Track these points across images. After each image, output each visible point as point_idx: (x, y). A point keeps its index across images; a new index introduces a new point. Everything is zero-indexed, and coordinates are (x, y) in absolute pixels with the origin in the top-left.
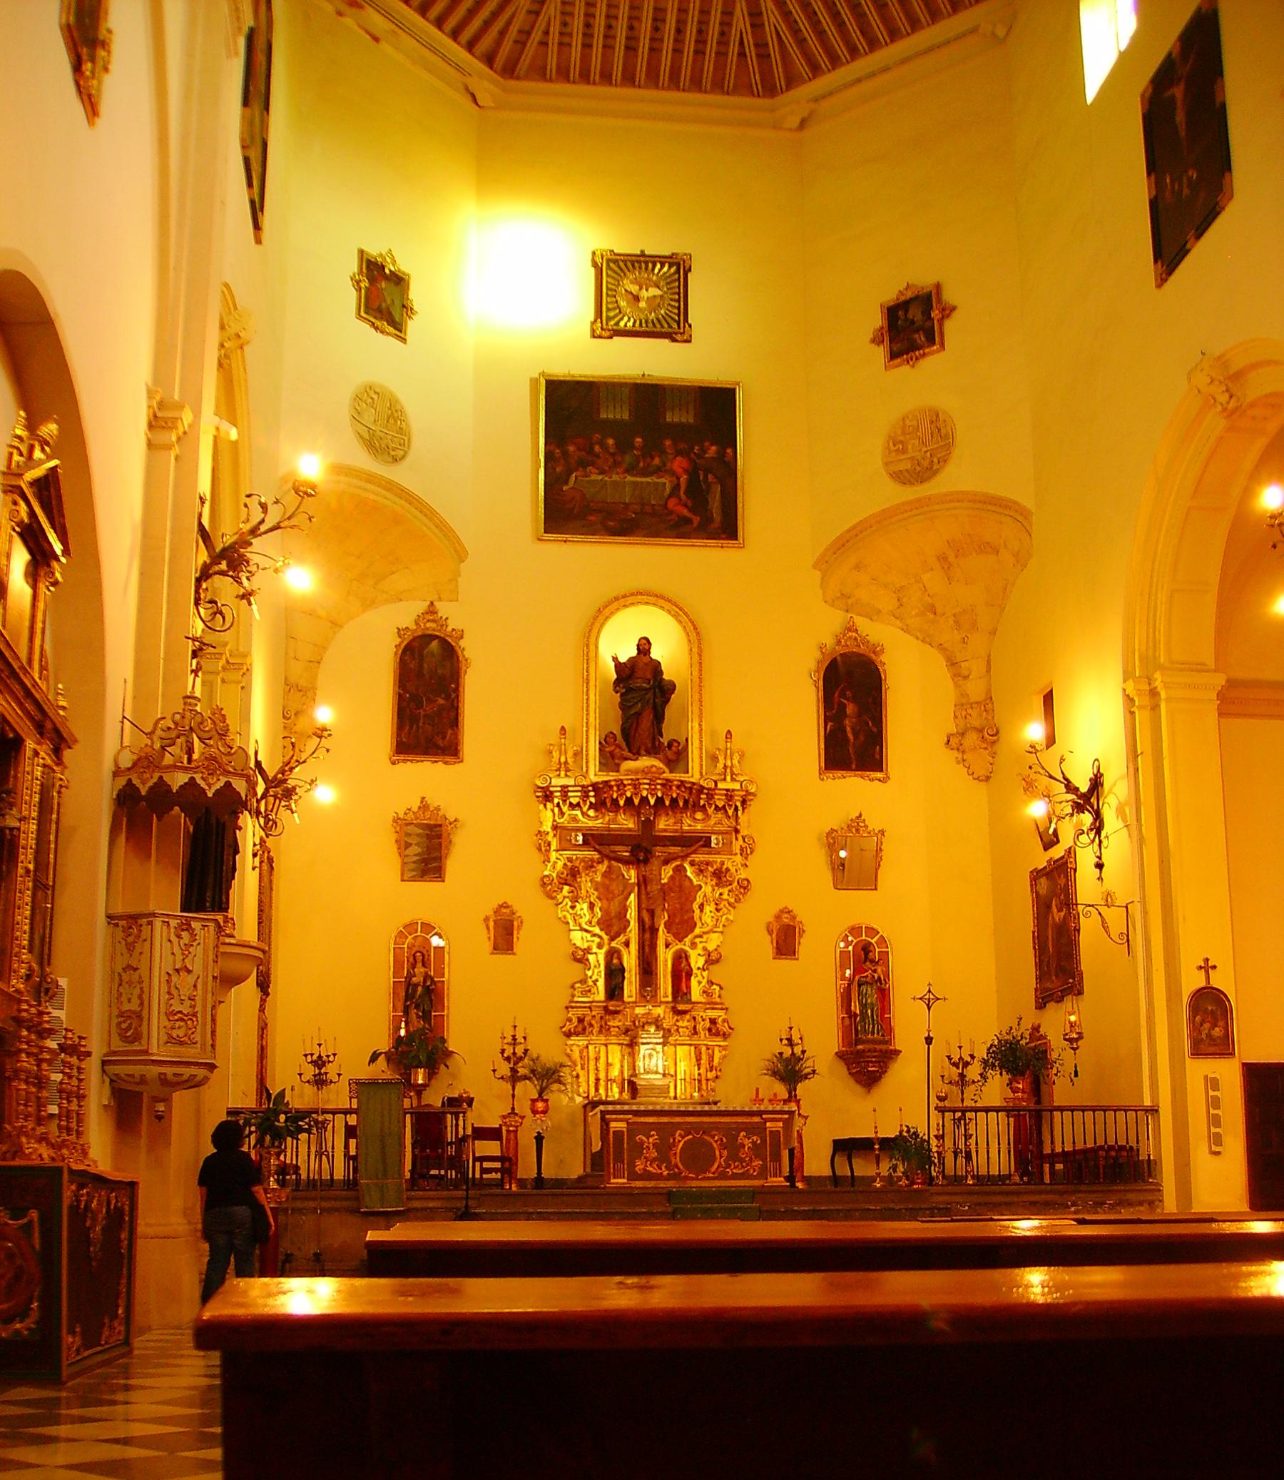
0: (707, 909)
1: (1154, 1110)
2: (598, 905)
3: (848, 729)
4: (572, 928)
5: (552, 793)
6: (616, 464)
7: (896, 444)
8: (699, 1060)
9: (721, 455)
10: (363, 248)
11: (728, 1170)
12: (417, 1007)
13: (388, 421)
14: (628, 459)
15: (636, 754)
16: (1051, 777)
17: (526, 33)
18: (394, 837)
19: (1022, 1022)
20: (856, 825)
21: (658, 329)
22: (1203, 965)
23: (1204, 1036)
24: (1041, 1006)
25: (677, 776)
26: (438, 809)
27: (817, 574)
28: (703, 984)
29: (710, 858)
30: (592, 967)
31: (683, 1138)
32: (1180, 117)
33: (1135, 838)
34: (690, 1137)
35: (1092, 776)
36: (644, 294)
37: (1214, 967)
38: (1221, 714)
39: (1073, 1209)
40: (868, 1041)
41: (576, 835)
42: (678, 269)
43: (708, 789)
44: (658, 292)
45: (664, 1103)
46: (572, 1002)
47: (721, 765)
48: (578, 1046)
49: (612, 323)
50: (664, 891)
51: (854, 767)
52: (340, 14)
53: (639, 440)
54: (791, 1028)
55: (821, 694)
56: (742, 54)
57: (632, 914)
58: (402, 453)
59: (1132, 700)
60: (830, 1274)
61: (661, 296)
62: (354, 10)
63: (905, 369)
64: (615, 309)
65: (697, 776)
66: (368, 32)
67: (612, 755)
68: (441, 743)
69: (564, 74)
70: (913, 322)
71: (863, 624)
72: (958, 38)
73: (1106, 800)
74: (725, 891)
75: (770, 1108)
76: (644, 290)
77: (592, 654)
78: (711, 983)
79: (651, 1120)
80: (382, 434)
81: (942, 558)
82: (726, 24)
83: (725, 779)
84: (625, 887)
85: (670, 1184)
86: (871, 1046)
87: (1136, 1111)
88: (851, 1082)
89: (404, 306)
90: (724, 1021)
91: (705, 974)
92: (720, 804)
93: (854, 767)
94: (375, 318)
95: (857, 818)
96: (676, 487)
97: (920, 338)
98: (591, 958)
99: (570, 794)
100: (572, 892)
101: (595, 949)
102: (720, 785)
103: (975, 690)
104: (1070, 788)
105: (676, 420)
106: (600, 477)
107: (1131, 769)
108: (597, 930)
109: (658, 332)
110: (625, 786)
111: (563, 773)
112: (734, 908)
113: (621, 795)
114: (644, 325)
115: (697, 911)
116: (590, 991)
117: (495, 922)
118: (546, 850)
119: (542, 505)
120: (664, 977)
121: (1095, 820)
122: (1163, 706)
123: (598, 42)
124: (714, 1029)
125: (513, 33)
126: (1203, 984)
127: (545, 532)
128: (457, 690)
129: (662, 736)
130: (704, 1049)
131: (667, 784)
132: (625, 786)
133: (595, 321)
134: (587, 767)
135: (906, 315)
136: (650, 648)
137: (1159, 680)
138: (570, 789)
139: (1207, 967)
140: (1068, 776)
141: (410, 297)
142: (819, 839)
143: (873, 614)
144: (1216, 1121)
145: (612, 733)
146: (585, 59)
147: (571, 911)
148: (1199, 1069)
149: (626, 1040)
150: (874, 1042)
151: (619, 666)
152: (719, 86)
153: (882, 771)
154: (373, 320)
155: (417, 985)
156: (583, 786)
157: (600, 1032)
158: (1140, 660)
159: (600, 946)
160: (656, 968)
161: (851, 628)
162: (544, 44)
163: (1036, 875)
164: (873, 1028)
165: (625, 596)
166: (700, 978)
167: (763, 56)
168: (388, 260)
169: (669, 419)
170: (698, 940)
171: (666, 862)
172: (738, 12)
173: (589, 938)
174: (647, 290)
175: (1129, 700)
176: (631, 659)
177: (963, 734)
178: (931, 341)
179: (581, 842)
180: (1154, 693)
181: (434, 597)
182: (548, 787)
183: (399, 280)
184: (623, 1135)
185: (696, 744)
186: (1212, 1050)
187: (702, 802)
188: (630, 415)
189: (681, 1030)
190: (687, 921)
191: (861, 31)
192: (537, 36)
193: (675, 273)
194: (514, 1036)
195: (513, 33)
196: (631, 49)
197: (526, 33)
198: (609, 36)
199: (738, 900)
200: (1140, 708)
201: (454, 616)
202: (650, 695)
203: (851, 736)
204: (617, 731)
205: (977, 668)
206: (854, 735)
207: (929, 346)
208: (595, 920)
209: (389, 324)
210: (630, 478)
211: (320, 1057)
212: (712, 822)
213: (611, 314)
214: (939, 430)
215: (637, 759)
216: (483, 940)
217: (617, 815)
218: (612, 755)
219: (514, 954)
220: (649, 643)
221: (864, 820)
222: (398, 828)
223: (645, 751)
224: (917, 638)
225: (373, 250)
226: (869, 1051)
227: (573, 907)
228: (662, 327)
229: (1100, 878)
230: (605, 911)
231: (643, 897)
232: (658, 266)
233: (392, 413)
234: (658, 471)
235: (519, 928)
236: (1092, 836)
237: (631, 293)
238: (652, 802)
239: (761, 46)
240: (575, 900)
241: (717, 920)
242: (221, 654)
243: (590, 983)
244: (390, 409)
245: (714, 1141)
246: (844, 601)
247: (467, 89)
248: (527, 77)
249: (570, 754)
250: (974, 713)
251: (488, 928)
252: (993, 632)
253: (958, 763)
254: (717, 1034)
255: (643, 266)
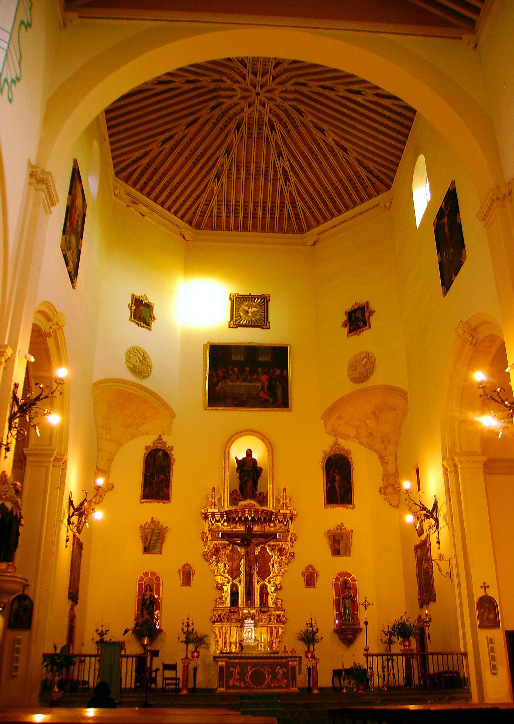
0: (276, 565)
1: (465, 654)
2: (228, 564)
3: (337, 487)
4: (216, 574)
5: (208, 515)
6: (238, 378)
7: (353, 367)
8: (271, 633)
9: (282, 373)
10: (134, 293)
11: (271, 684)
12: (147, 609)
13: (142, 362)
14: (243, 376)
15: (245, 499)
16: (415, 504)
17: (204, 213)
18: (140, 534)
19: (406, 614)
20: (341, 527)
21: (256, 324)
22: (483, 585)
23: (485, 618)
24: (421, 607)
25: (263, 508)
26: (159, 522)
27: (322, 422)
28: (274, 599)
29: (277, 543)
30: (225, 591)
31: (251, 669)
32: (446, 229)
33: (451, 529)
34: (254, 669)
35: (434, 503)
36: (250, 310)
37: (488, 587)
38: (485, 474)
39: (429, 702)
40: (347, 625)
41: (218, 534)
42: (264, 301)
43: (275, 513)
44: (256, 309)
45: (254, 653)
46: (216, 607)
47: (281, 503)
48: (218, 627)
49: (237, 322)
50: (256, 558)
51: (339, 502)
52: (128, 206)
53: (247, 368)
54: (311, 619)
55: (325, 472)
56: (289, 218)
57: (242, 569)
58: (148, 374)
59: (447, 469)
60: (105, 709)
61: (257, 311)
62: (135, 205)
63: (355, 337)
64: (238, 316)
65: (271, 507)
66: (140, 213)
67: (235, 499)
68: (162, 494)
69: (219, 227)
70: (358, 318)
71: (341, 441)
72: (372, 208)
73: (440, 513)
74: (284, 557)
75: (290, 655)
76: (250, 309)
77: (227, 456)
78: (277, 599)
79: (237, 661)
80: (139, 367)
81: (374, 413)
82: (282, 207)
83: (283, 509)
84: (239, 556)
85: (245, 691)
86: (347, 627)
87: (457, 654)
88: (340, 643)
89: (150, 316)
90: (283, 616)
91: (274, 594)
92: (281, 520)
93: (339, 502)
94: (138, 321)
95: (341, 525)
96: (263, 387)
97: (361, 324)
98: (225, 588)
99: (216, 516)
100: (216, 558)
101: (226, 584)
102: (281, 511)
103: (391, 468)
104: (423, 508)
105: (263, 360)
106: (231, 383)
107: (448, 499)
108: (227, 575)
109: (259, 325)
110: (238, 512)
111: (213, 507)
112: (288, 565)
113: (237, 516)
114: (250, 322)
115: (271, 567)
116: (224, 602)
117: (183, 572)
118: (205, 540)
119: (207, 395)
120: (257, 596)
121: (436, 522)
122: (459, 471)
123: (232, 215)
124: (278, 619)
125: (199, 212)
126: (483, 594)
127: (208, 406)
128: (169, 472)
129: (257, 491)
130: (274, 628)
131: (256, 511)
132: (238, 512)
133: (230, 321)
134: (224, 504)
135: (355, 315)
136: (252, 453)
137: (457, 460)
138: (215, 513)
139: (485, 587)
140: (423, 503)
141: (153, 313)
142: (325, 534)
143: (346, 437)
144: (493, 658)
145: (235, 489)
146: (228, 222)
147: (216, 567)
148: (484, 634)
149: (239, 625)
150: (350, 625)
151: (238, 461)
152: (281, 230)
153: (352, 504)
154: (137, 322)
155: (147, 600)
156: (221, 513)
157: (228, 621)
158: (449, 452)
159: (228, 582)
160: (253, 592)
161: (337, 443)
162: (211, 216)
163: (417, 548)
164: (349, 618)
165: (241, 432)
166: (272, 596)
167: (298, 218)
168: (145, 298)
169: (260, 360)
170: (271, 580)
171: (257, 545)
172: (286, 202)
173: (224, 579)
174: (251, 309)
175: (445, 469)
176: (244, 459)
177: (386, 488)
178: (365, 325)
179: (220, 537)
180: (455, 466)
181: (161, 433)
182: (206, 513)
183: (149, 306)
184: (224, 668)
185: (271, 493)
186: (489, 625)
187: (273, 519)
188: (244, 357)
189: (263, 620)
190: (266, 571)
191: (334, 208)
192: (208, 213)
193: (263, 302)
194: (188, 623)
195: (199, 212)
196: (245, 217)
197: (204, 213)
198: (236, 213)
199: (289, 562)
200: (450, 472)
201: (169, 441)
202: (251, 473)
203: (338, 490)
204: (238, 489)
205: (391, 459)
206: (339, 489)
207: (364, 327)
208: (226, 571)
209: (144, 323)
210: (244, 384)
211: (102, 631)
212: (278, 527)
213: (237, 318)
214: (369, 360)
215: (245, 501)
216: (177, 580)
217: (236, 525)
218: (235, 499)
219: (191, 586)
220: (251, 452)
221: (344, 526)
222: (142, 531)
223: (249, 497)
224: (366, 447)
225: (138, 294)
226: (347, 629)
227: (217, 565)
228: (258, 323)
229: (439, 548)
230: (231, 567)
231: (247, 560)
232: (257, 299)
233: (144, 359)
234: (255, 381)
235: (193, 574)
236: (434, 529)
237: (245, 310)
238: (250, 519)
239: (297, 215)
240: (218, 562)
241: (280, 570)
242: (52, 454)
243: (224, 599)
244: (143, 356)
245: (265, 670)
246: (334, 432)
247: (181, 234)
248: (204, 229)
249: (216, 498)
250: (391, 478)
251: (180, 575)
252: (397, 444)
253: (385, 500)
254: (280, 622)
255: (250, 299)
